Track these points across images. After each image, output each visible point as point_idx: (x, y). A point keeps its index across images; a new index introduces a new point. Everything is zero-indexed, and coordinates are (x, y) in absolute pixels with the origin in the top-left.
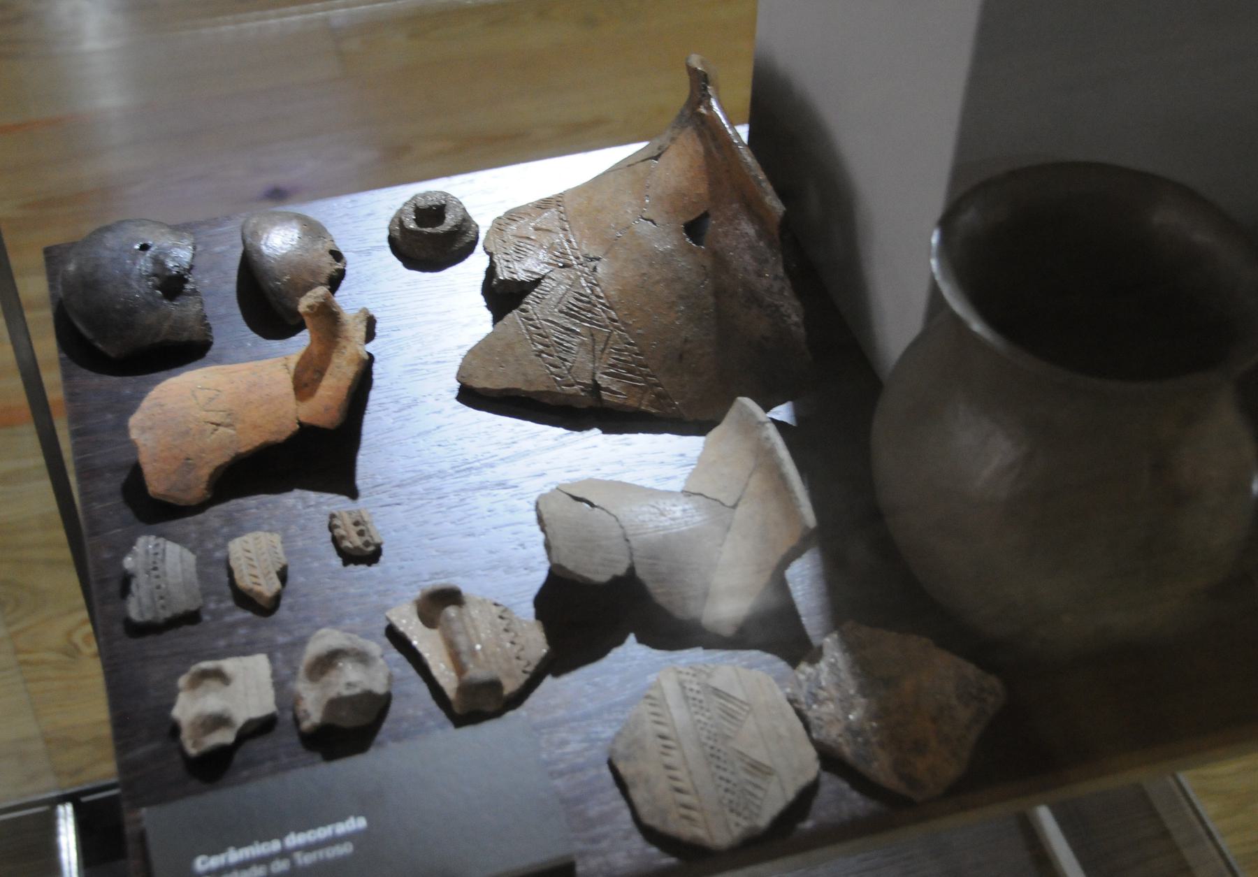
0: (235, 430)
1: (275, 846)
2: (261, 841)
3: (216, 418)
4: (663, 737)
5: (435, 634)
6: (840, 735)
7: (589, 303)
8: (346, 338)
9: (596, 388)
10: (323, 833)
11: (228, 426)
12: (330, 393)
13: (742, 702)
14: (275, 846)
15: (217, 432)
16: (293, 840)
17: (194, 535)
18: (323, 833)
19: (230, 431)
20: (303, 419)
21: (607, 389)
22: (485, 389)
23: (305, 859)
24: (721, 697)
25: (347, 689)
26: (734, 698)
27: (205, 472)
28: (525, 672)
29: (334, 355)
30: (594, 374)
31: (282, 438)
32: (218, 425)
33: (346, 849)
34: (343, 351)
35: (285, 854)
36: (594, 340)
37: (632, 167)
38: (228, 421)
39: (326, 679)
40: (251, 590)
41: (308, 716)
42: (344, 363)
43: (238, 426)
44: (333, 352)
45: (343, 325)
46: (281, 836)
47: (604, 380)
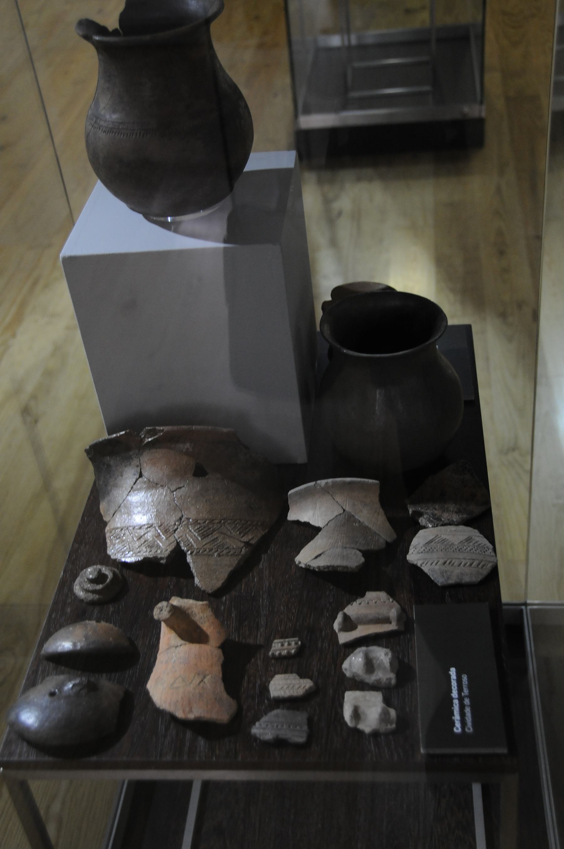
0: (208, 675)
1: (456, 702)
2: (453, 706)
3: (197, 680)
4: (445, 563)
5: (360, 627)
6: (459, 516)
7: (204, 527)
8: (188, 609)
9: (247, 544)
10: (454, 684)
11: (204, 677)
12: (212, 628)
13: (435, 538)
14: (456, 702)
15: (206, 682)
16: (455, 694)
17: (460, 516)
18: (454, 684)
19: (208, 678)
20: (218, 645)
21: (250, 540)
22: (223, 584)
23: (466, 691)
24: (432, 542)
25: (388, 656)
26: (433, 539)
27: (225, 695)
28: (392, 602)
29: (193, 618)
30: (241, 541)
31: (222, 658)
32: (202, 681)
33: (465, 678)
34: (194, 613)
35: (461, 699)
36: (224, 534)
37: (129, 491)
38: (201, 677)
39: (375, 666)
40: (306, 691)
41: (390, 679)
42: (201, 615)
43: (207, 672)
44: (191, 618)
45: (181, 606)
46: (452, 699)
47: (245, 539)
